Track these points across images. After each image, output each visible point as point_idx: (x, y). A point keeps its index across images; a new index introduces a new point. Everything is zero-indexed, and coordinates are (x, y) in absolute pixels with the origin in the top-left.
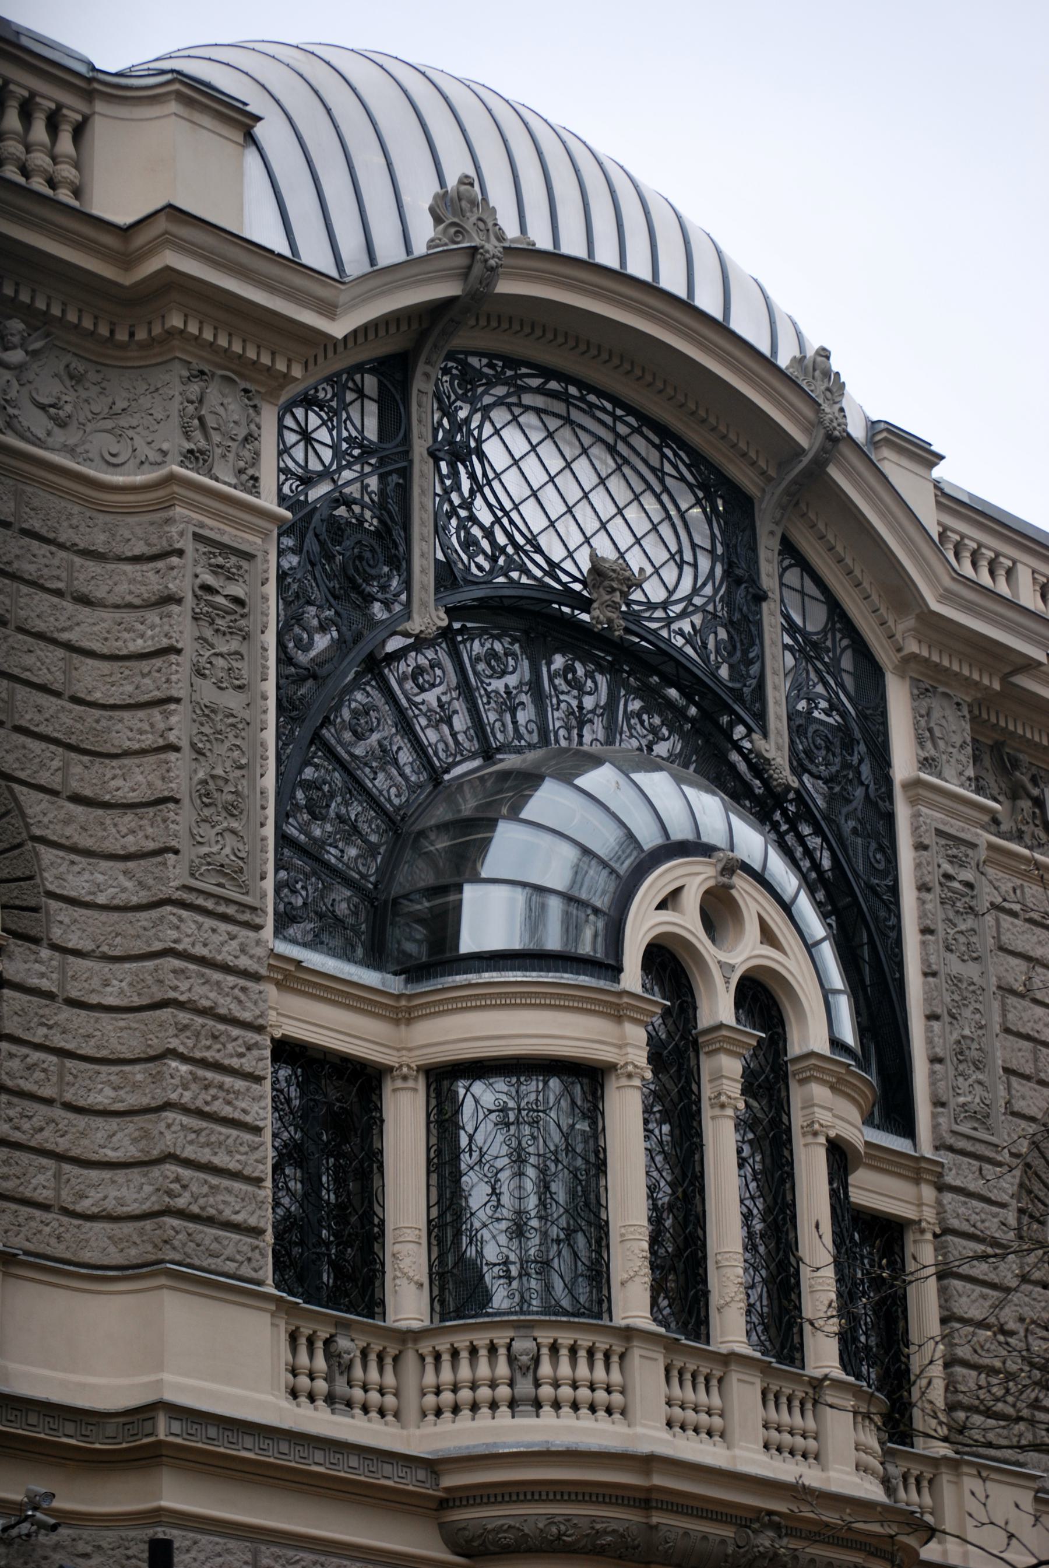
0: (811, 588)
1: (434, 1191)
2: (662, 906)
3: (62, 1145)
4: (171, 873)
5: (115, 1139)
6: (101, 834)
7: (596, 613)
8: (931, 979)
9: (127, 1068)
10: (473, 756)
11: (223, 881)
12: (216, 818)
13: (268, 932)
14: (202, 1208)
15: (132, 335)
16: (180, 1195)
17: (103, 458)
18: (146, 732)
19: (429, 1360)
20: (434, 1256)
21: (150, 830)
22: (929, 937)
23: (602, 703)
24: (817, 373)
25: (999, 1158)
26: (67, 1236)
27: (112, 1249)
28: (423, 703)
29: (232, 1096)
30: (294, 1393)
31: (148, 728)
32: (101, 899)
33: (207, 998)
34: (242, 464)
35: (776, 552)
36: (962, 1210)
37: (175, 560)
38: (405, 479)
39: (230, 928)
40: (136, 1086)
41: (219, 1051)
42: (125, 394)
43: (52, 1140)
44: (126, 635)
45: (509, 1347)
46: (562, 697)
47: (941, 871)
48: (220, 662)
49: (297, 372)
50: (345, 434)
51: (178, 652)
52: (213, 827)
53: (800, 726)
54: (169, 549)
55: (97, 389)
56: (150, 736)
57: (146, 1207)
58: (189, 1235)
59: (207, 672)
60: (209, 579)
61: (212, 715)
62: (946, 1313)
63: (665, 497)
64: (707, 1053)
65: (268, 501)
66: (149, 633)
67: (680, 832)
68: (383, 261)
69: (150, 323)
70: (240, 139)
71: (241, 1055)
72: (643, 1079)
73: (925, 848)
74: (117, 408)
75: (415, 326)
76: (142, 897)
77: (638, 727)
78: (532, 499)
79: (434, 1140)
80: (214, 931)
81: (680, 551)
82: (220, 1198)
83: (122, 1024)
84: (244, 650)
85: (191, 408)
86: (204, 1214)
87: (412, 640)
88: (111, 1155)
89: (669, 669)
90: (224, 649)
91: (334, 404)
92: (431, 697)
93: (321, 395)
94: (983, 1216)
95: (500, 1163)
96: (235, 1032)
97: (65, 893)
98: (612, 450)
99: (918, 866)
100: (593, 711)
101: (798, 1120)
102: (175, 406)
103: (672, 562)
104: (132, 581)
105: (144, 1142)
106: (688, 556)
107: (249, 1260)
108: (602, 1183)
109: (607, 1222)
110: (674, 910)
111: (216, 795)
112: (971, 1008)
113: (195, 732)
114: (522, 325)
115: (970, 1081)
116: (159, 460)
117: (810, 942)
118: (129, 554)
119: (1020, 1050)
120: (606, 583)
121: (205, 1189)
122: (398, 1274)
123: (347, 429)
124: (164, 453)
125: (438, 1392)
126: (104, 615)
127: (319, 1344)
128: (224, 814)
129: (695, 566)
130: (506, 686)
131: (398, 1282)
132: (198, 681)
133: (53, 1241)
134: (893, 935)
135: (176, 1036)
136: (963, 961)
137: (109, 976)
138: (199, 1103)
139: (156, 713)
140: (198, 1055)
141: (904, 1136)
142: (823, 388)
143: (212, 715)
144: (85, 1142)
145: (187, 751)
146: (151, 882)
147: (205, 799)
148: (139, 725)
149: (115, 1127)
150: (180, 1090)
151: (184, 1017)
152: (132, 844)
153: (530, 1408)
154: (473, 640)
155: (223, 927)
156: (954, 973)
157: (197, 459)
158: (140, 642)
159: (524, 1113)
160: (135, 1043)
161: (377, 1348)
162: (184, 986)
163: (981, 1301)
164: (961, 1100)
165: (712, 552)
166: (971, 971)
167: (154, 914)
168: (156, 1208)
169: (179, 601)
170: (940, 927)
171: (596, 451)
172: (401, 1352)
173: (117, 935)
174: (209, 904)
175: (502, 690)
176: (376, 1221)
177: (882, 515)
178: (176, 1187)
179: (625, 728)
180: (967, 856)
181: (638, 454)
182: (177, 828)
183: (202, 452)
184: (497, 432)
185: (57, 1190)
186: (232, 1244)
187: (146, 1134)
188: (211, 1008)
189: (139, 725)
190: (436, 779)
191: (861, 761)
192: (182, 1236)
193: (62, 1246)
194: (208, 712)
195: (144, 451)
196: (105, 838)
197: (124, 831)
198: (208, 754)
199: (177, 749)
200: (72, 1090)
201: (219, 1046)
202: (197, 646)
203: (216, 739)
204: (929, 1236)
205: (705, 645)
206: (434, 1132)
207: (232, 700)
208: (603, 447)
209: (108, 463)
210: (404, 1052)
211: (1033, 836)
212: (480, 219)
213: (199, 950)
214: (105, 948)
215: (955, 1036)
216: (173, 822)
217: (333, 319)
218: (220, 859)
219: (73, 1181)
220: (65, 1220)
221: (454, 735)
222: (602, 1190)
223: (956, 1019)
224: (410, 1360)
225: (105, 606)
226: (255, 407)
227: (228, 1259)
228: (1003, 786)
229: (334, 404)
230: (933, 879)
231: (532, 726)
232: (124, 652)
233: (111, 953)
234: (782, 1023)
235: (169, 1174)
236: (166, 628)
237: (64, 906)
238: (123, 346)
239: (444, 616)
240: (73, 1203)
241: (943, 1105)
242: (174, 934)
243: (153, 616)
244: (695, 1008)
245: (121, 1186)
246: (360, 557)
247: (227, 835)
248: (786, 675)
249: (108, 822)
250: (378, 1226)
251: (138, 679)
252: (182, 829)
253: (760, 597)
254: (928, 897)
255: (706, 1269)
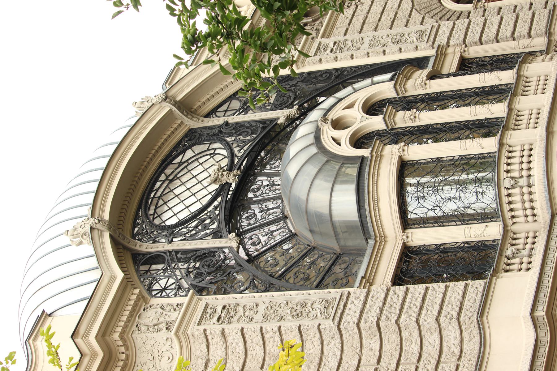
0: (224, 107)
1: (450, 224)
2: (339, 144)
3: (434, 362)
4: (328, 326)
5: (431, 342)
6: (313, 355)
7: (231, 181)
8: (370, 54)
9: (404, 339)
10: (286, 223)
11: (331, 307)
12: (307, 311)
13: (351, 290)
14: (457, 306)
15: (123, 353)
16: (452, 315)
17: (171, 362)
18: (274, 339)
19: (514, 220)
20: (476, 222)
21: (312, 336)
22: (354, 56)
23: (266, 178)
24: (142, 106)
25: (437, 26)
26: (469, 358)
27: (474, 340)
28: (265, 241)
29: (414, 299)
30: (528, 269)
31: (273, 339)
32: (339, 353)
33: (376, 310)
34: (172, 310)
35: (209, 119)
36: (456, 37)
37: (208, 332)
38: (180, 252)
39: (349, 303)
40: (410, 335)
41: (396, 304)
42: (146, 355)
43: (432, 366)
44: (237, 350)
45: (509, 189)
46: (264, 192)
47: (329, 53)
48: (247, 314)
49: (137, 291)
50: (162, 274)
51: (243, 329)
52: (310, 312)
53: (275, 106)
54: (204, 334)
55: (144, 366)
56: (275, 338)
57: (457, 328)
58: (467, 310)
59: (251, 318)
60: (215, 318)
61: (267, 315)
62: (495, 40)
63: (189, 161)
64: (395, 125)
65: (186, 300)
66: (236, 341)
67: (311, 139)
68: (96, 265)
69: (118, 346)
70: (50, 318)
71: (398, 296)
72: (405, 145)
73: (321, 60)
74: (151, 358)
75: (121, 250)
76: (337, 336)
77: (275, 165)
78: (189, 208)
79: (431, 225)
80: (350, 309)
81: (210, 154)
82: (453, 300)
83: (387, 342)
84: (243, 305)
85: (150, 329)
86: (459, 305)
87: (241, 246)
88: (438, 342)
89: (253, 155)
90: (242, 312)
91: (150, 279)
92: (263, 239)
93: (147, 283)
94: (458, 30)
95: (439, 198)
96: (389, 299)
97: (336, 367)
98: (171, 181)
99: (327, 61)
100: (269, 181)
101: (420, 92)
102: (150, 335)
103: (214, 157)
104: (217, 349)
105: (432, 330)
106: (212, 152)
107: (477, 288)
108: (445, 159)
109: (460, 156)
110: (340, 140)
111: (298, 311)
112: (381, 39)
113: (274, 321)
114: (122, 213)
115: (408, 38)
116: (170, 340)
117: (353, 91)
118: (206, 350)
119: (398, 24)
120: (220, 177)
121: (450, 306)
122: (482, 235)
123: (160, 274)
124: (167, 339)
125: (527, 216)
126: (230, 358)
127: (509, 261)
128: (305, 308)
129: (215, 149)
130: (259, 212)
131: (485, 235)
132: (254, 321)
133: (471, 362)
134: (353, 69)
135: (390, 320)
136: (363, 43)
137: (368, 348)
138: (417, 310)
139: (266, 336)
140: (398, 312)
141: (429, 60)
142: (147, 103)
143: (267, 315)
144: (433, 353)
145: (281, 323)
146: (331, 334)
147: (299, 316)
148: (271, 342)
149: (427, 342)
150: (411, 318)
151: (383, 318)
152: (317, 342)
153: (531, 179)
154: (241, 226)
155: (349, 306)
156: (368, 47)
157: (169, 326)
158: (240, 344)
159: (419, 190)
160: (394, 337)
161: (510, 240)
162: (371, 318)
163: (490, 29)
164: (415, 40)
165: (210, 144)
166: (367, 41)
167: (343, 332)
168: (457, 324)
169: (223, 330)
170: (350, 53)
171: (172, 186)
172: (512, 232)
173: (352, 346)
174: (340, 311)
175: (261, 214)
176: (462, 245)
177: (195, 80)
178: (449, 317)
179: (276, 169)
180: (324, 45)
181: (173, 172)
182: (310, 325)
183: (167, 324)
184: (164, 222)
185: (451, 362)
186: (471, 295)
187: (429, 330)
188: (380, 308)
189: (271, 342)
190: (294, 235)
191: (289, 85)
192: (468, 313)
193: (473, 359)
194: (266, 317)
195: (167, 347)
196: (315, 354)
197: (312, 346)
198: (282, 315)
199: (280, 327)
200: (413, 359)
201: (395, 304)
202: (241, 321)
203: (276, 313)
204: (466, 49)
205: (244, 141)
206: (427, 225)
207: (261, 309)
208: (171, 184)
209: (172, 359)
210: (397, 238)
211: (318, 25)
212: (81, 227)
213: (358, 314)
214: (358, 351)
215: (391, 44)
216: (308, 327)
217: (117, 277)
218: (322, 308)
219: (448, 357)
220: (463, 359)
221: (278, 230)
222: (448, 159)
223: (385, 44)
224: (514, 228)
225: (226, 358)
226: (150, 306)
227: (477, 296)
228: (299, 37)
229: (150, 279)
230: (333, 55)
231: (274, 202)
232: (244, 350)
233: (360, 348)
234: (384, 100)
235: (444, 319)
236: (234, 334)
237: (341, 367)
238: (127, 357)
239: (231, 234)
240: (456, 356)
241: (417, 47)
242: (351, 324)
243: (230, 340)
244: (378, 130)
245: (449, 338)
246: (209, 266)
247: (313, 307)
248: (255, 113)
249: (309, 352)
250: (464, 244)
251: (254, 344)
252: (311, 323)
253: (227, 124)
254: (339, 58)
255: (477, 120)
